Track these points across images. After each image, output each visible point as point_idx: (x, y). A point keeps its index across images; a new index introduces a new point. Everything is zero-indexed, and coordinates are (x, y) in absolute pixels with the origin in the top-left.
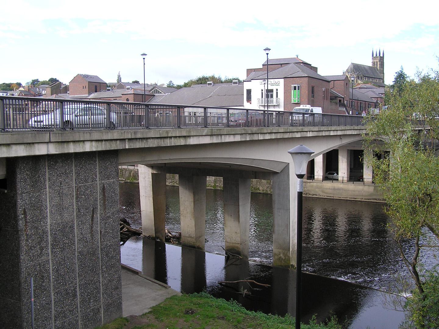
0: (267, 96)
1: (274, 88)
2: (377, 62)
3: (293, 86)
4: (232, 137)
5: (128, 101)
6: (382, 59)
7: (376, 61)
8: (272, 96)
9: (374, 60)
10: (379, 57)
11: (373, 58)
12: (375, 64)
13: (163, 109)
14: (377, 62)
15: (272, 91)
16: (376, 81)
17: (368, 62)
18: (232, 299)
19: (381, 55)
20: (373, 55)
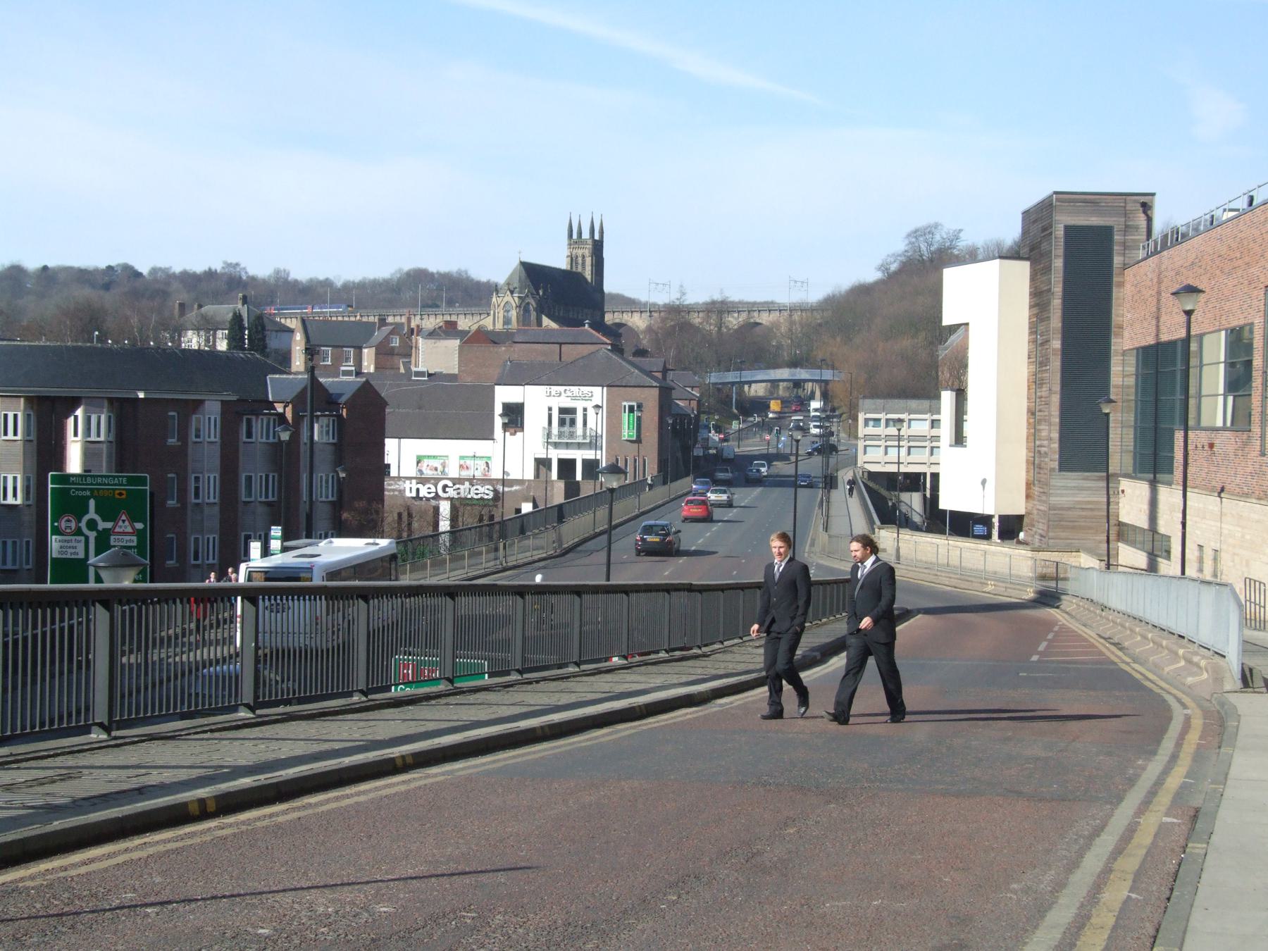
0: (562, 423)
1: (579, 406)
2: (583, 257)
3: (627, 404)
4: (1259, 409)
5: (102, 453)
6: (598, 247)
7: (580, 252)
8: (573, 422)
9: (574, 252)
10: (590, 242)
11: (570, 244)
12: (577, 263)
13: (1119, 444)
14: (583, 257)
15: (572, 411)
16: (575, 316)
17: (557, 258)
18: (890, 504)
19: (597, 237)
20: (570, 235)
